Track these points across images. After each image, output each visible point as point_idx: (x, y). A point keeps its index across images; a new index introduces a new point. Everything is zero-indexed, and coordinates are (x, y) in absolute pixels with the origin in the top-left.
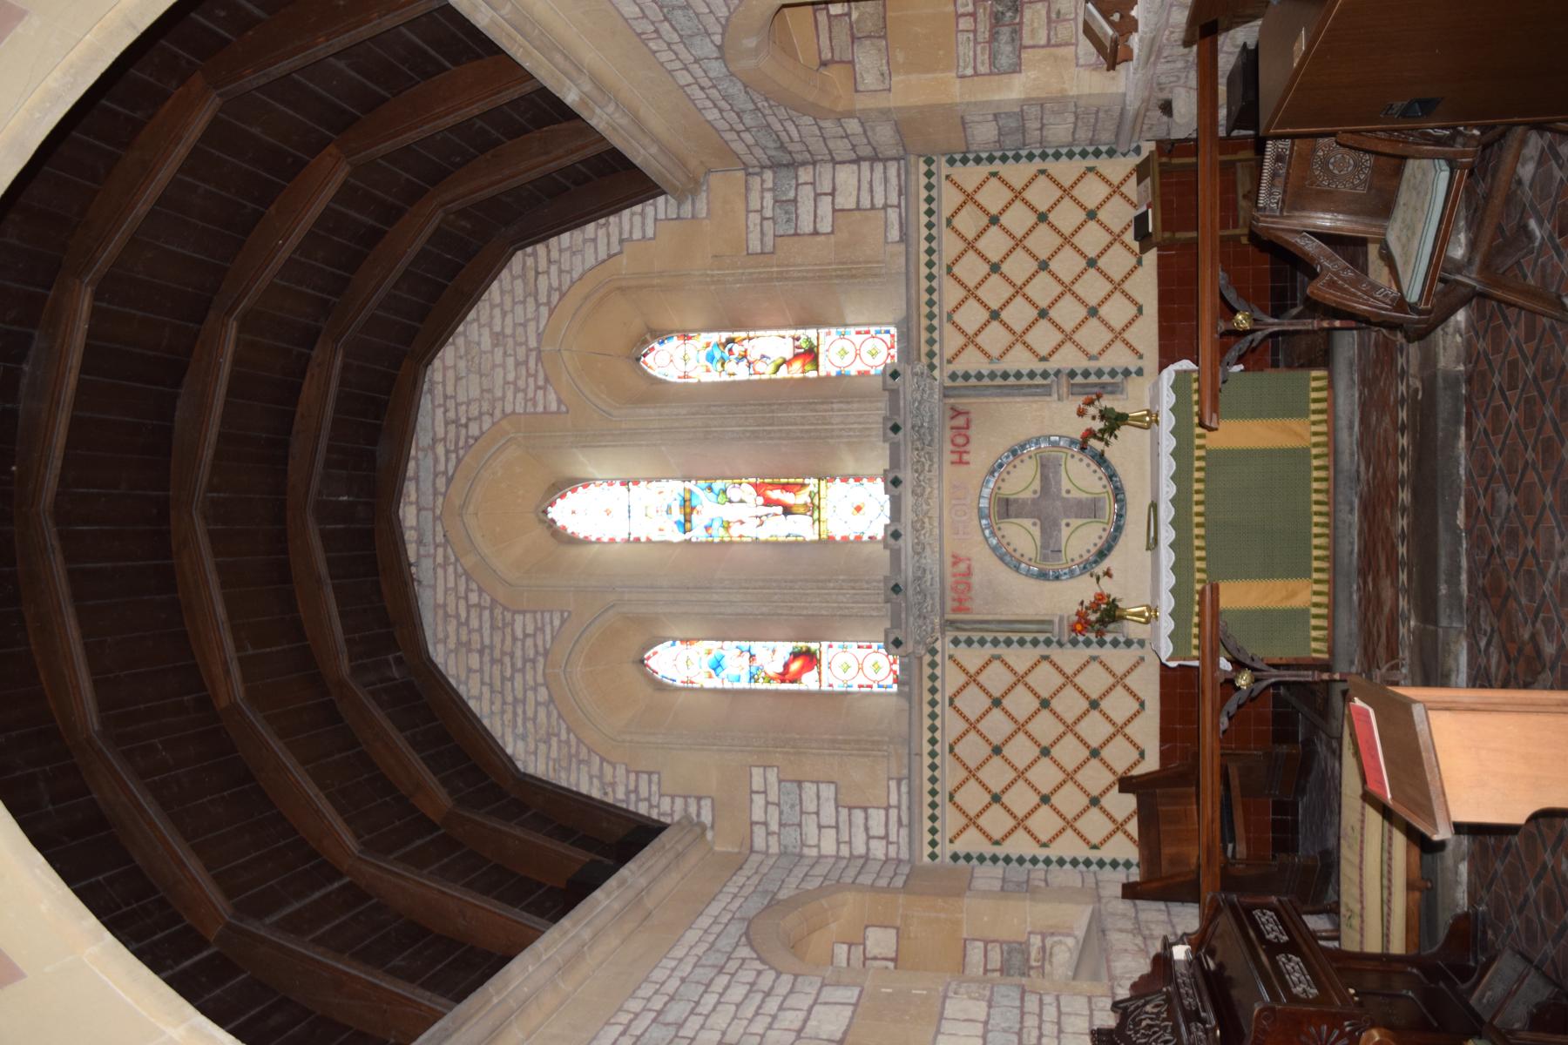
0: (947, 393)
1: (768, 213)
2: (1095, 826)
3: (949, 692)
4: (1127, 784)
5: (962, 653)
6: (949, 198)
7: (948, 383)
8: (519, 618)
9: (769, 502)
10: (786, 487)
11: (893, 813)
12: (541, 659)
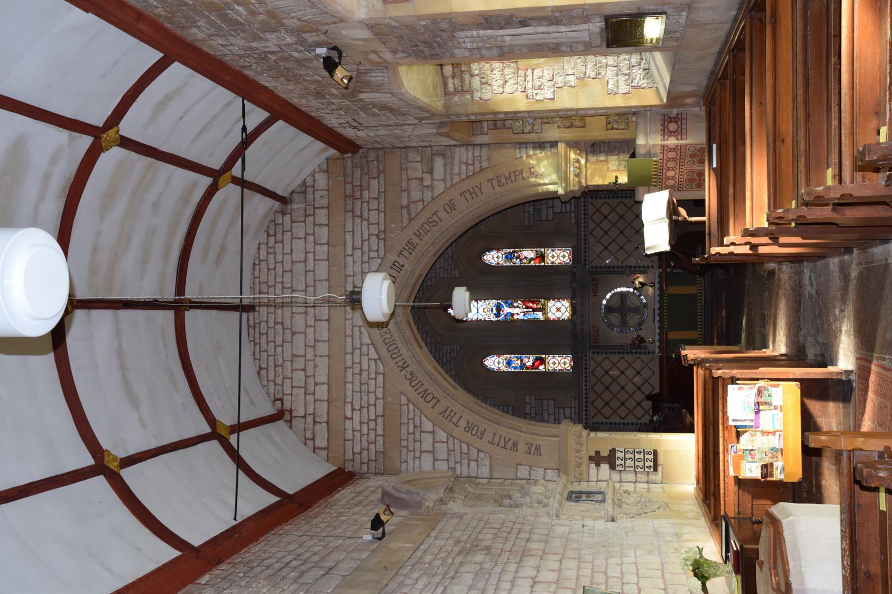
1: (531, 213)
2: (639, 412)
4: (649, 397)
6: (591, 210)
7: (591, 270)
8: (445, 347)
10: (533, 302)
11: (573, 409)
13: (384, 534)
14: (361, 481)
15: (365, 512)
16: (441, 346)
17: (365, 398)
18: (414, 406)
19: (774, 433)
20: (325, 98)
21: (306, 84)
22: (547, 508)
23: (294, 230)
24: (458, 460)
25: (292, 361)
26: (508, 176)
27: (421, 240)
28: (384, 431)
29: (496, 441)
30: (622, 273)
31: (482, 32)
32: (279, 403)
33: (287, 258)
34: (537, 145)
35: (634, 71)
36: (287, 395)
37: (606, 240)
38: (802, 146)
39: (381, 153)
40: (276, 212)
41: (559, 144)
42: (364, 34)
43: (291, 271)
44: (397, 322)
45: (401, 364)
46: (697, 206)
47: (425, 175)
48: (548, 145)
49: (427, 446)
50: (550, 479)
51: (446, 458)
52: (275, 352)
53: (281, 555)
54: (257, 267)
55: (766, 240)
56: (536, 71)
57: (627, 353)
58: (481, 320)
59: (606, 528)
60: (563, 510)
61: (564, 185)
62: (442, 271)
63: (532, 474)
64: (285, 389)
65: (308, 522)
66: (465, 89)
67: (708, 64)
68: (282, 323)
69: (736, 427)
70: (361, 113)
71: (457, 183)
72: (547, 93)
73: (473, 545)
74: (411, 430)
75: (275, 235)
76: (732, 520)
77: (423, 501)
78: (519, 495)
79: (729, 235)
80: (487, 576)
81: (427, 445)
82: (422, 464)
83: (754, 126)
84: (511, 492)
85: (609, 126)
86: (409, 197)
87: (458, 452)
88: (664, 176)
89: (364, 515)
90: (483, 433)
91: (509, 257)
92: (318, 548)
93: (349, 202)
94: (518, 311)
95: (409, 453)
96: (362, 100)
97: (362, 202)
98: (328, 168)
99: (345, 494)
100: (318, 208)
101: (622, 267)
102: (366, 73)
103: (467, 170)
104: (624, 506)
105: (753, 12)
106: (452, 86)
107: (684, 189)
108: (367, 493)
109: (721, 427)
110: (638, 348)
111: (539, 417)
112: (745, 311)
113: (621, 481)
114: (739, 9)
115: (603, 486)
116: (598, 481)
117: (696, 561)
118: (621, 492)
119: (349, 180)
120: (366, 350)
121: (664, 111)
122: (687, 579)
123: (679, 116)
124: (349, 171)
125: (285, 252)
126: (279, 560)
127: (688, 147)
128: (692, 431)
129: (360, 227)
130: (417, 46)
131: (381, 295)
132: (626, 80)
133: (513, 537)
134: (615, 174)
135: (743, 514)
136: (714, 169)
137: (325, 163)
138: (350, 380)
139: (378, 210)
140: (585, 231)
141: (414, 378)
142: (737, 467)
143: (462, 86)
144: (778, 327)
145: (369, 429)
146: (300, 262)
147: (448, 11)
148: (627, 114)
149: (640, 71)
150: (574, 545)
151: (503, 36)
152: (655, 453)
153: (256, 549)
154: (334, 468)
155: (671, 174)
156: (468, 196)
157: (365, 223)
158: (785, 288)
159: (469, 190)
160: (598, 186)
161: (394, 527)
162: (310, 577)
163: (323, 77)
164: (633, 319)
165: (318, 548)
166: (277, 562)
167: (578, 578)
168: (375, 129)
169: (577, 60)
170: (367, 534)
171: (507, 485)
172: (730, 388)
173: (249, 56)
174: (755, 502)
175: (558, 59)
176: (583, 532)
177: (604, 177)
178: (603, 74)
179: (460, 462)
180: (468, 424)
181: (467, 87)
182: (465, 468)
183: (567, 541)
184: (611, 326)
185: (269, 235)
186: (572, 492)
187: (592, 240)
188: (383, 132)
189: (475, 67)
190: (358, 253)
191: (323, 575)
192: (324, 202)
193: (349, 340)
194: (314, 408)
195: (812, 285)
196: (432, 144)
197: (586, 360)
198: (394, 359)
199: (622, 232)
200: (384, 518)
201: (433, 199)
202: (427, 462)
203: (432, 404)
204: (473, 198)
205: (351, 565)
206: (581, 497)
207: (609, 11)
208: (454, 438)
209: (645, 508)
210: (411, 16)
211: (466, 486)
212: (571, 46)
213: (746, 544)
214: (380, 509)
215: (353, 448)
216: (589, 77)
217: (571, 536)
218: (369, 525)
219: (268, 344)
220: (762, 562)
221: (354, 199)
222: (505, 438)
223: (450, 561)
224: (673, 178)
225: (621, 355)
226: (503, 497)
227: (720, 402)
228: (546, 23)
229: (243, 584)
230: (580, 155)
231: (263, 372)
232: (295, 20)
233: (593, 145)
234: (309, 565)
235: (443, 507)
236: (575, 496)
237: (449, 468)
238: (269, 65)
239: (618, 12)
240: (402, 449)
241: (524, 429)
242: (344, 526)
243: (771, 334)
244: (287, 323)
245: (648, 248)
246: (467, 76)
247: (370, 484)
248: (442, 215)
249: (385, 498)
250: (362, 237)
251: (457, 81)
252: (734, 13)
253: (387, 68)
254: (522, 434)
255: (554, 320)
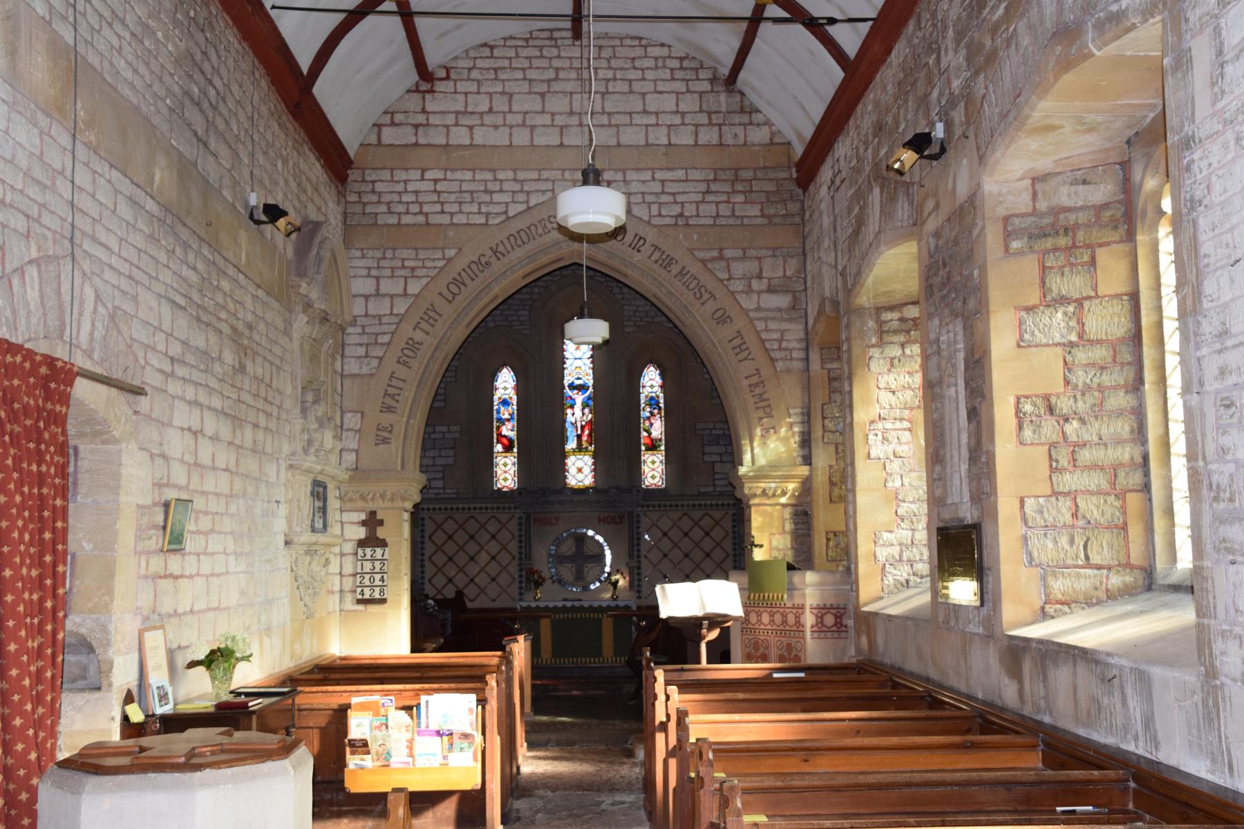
0: (631, 514)
1: (713, 432)
2: (440, 581)
3: (498, 516)
4: (460, 594)
5: (515, 522)
6: (717, 514)
7: (635, 514)
8: (527, 313)
9: (583, 427)
10: (590, 435)
11: (442, 491)
12: (507, 324)
13: (258, 222)
14: (333, 192)
15: (290, 196)
16: (527, 307)
17: (453, 197)
18: (442, 268)
19: (411, 755)
20: (874, 138)
21: (894, 110)
22: (301, 452)
23: (688, 96)
24: (367, 330)
25: (503, 93)
26: (764, 397)
27: (676, 277)
28: (406, 225)
29: (394, 383)
30: (631, 556)
31: (961, 356)
32: (444, 75)
33: (649, 86)
34: (806, 437)
35: (906, 567)
36: (455, 85)
37: (675, 534)
38: (797, 783)
39: (797, 220)
40: (715, 70)
41: (807, 467)
42: (962, 190)
43: (631, 92)
44: (559, 243)
45: (501, 248)
46: (721, 653)
47: (765, 281)
48: (806, 452)
49: (386, 286)
50: (343, 458)
51: (370, 312)
52: (516, 68)
53: (224, 72)
54: (637, 43)
55: (673, 741)
56: (907, 433)
57: (520, 565)
58: (565, 363)
59: (275, 533)
60: (300, 474)
61: (751, 474)
62: (632, 308)
63: (349, 433)
64: (463, 82)
65: (272, 115)
66: (884, 336)
67: (912, 665)
68: (557, 79)
69: (418, 706)
70: (853, 190)
71: (755, 327)
72: (878, 450)
73: (245, 348)
74: (408, 264)
75: (681, 68)
76: (290, 701)
77: (307, 279)
78: (319, 414)
79: (679, 693)
80: (202, 367)
81: (387, 286)
82: (360, 279)
83: (828, 723)
84: (323, 403)
85: (832, 535)
86: (735, 259)
87: (378, 329)
88: (762, 610)
89: (285, 194)
90: (405, 364)
91: (653, 402)
92: (235, 128)
93: (729, 175)
94: (577, 415)
95: (376, 261)
96: (871, 190)
97: (728, 193)
98: (777, 144)
99: (315, 169)
100: (720, 130)
101: (639, 556)
102: (908, 192)
103: (773, 340)
104: (308, 559)
105: (980, 721)
106: (889, 318)
107: (744, 637)
108: (318, 200)
109: (418, 686)
110: (528, 580)
111: (429, 444)
112: (579, 721)
113: (342, 555)
114: (985, 703)
115: (336, 530)
116: (342, 523)
117: (233, 652)
118: (328, 555)
119: (760, 174)
120: (520, 200)
121: (851, 608)
122: (208, 642)
123: (843, 629)
124: (772, 175)
125: (658, 83)
126: (216, 70)
127: (802, 641)
128: (414, 649)
129: (693, 190)
130: (945, 265)
131: (594, 213)
132: (893, 557)
133: (260, 404)
134: (766, 544)
135: (299, 716)
136: (771, 674)
137: (783, 141)
138: (478, 177)
139: (718, 215)
140: (688, 506)
141: (481, 268)
142: (363, 707)
143: (888, 332)
144: (556, 763)
145: (408, 203)
146: (644, 105)
147: (992, 307)
148: (849, 560)
149: (905, 575)
150: (250, 489)
151: (956, 385)
152: (382, 601)
153: (230, 37)
154: (352, 153)
155: (766, 618)
156: (737, 342)
157: (699, 197)
158: (608, 771)
159: (745, 343)
160: (749, 520)
161: (269, 238)
162: (192, 114)
163: (903, 134)
164: (567, 572)
165: (235, 128)
166: (213, 68)
167: (204, 493)
168: (831, 211)
169: (922, 492)
170: (258, 197)
171: (333, 396)
172: (472, 698)
173: (934, 25)
174: (315, 731)
175: (924, 464)
176: (269, 502)
177: (761, 529)
178: (902, 525)
179: (364, 333)
180: (418, 343)
181: (887, 338)
182: (357, 339)
183: (256, 479)
184: (558, 542)
185: (681, 59)
186: (325, 488)
187: (675, 515)
188: (826, 221)
189: (915, 349)
190: (657, 187)
191: (196, 134)
192: (728, 139)
193: (534, 175)
194: (436, 126)
195: (613, 804)
196: (809, 291)
197: (510, 508)
198: (508, 238)
199: (686, 556)
200: (282, 222)
201: (732, 293)
202: (363, 286)
203: (445, 292)
204: (734, 348)
205: (211, 174)
206: (319, 500)
207: (987, 529)
208: (398, 324)
209: (306, 587)
210: (985, 257)
211: (331, 341)
212: (940, 479)
213: (258, 718)
214: (294, 217)
215: (381, 181)
216: (898, 506)
217: (264, 485)
218: (271, 201)
219: (526, 58)
220: (231, 735)
221: (733, 182)
222: (399, 395)
223: (223, 315)
224: (759, 621)
225: (517, 556)
226: (317, 391)
227: (453, 685)
228: (972, 444)
229: (179, 16)
230: (793, 495)
231: (487, 52)
232: (983, 91)
233: (806, 514)
234: (210, 114)
235: (299, 308)
236: (319, 491)
237: (355, 317)
238: (922, 56)
239: (984, 542)
240: (382, 251)
241: (412, 421)
242: (268, 166)
243: (548, 754)
244: (556, 86)
245: (663, 588)
246: (902, 338)
247: (331, 205)
248: (710, 306)
249: (310, 226)
250: (679, 193)
251: (895, 325)
252: (980, 696)
253: (915, 224)
254: (405, 419)
255: (565, 464)
